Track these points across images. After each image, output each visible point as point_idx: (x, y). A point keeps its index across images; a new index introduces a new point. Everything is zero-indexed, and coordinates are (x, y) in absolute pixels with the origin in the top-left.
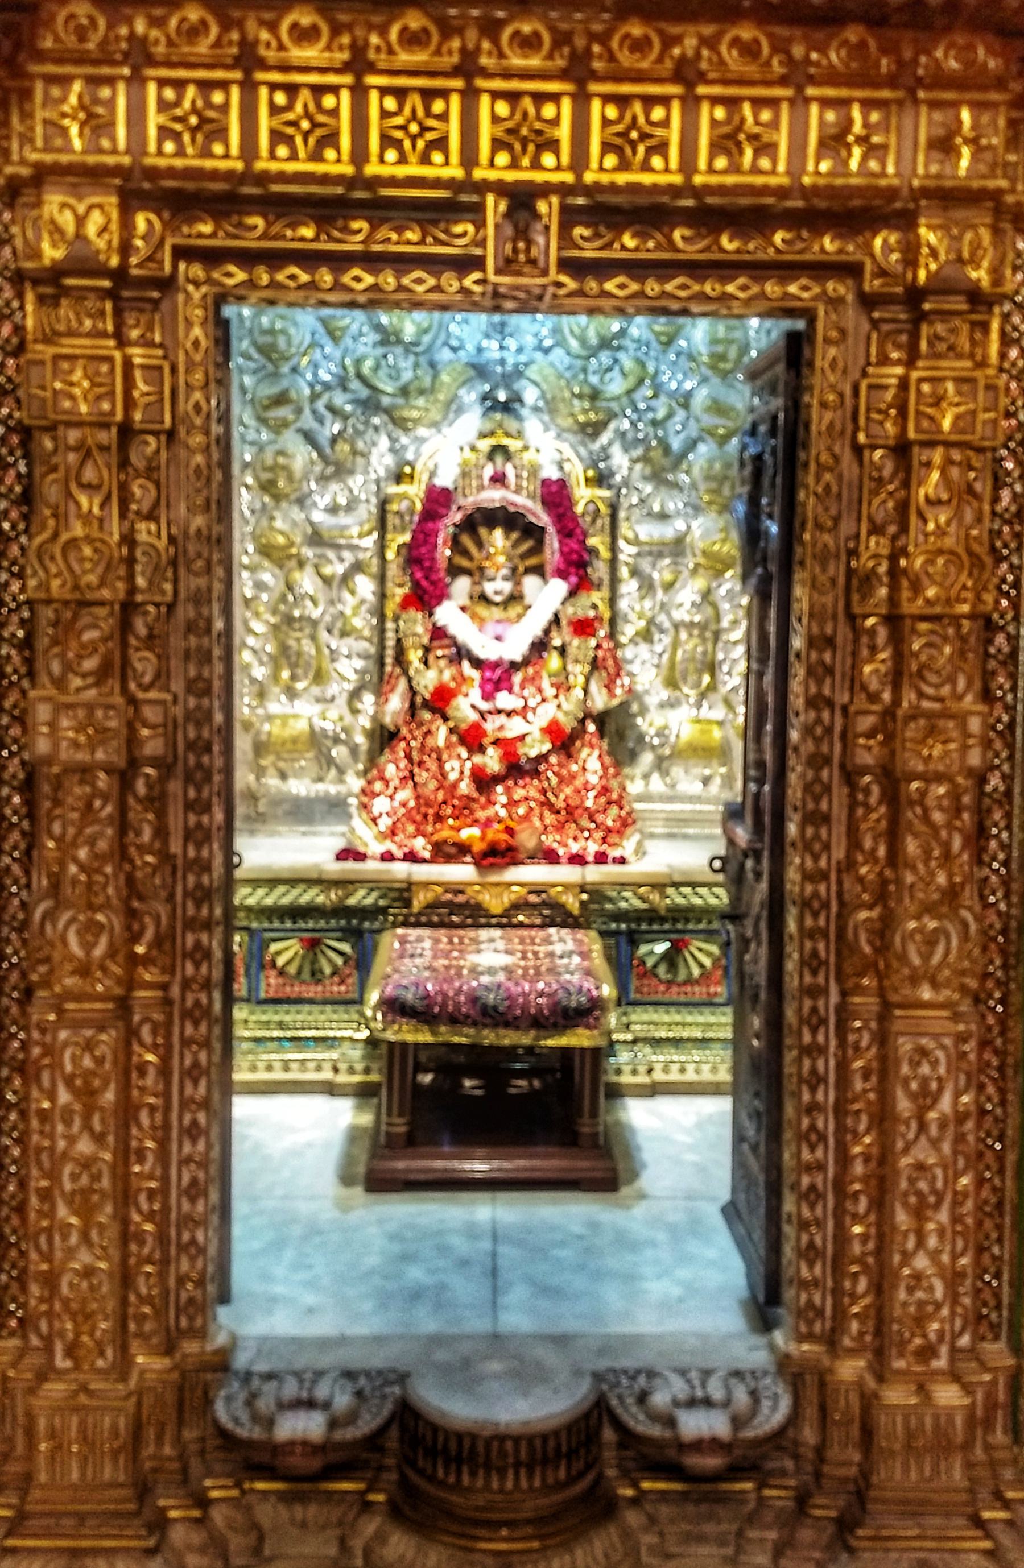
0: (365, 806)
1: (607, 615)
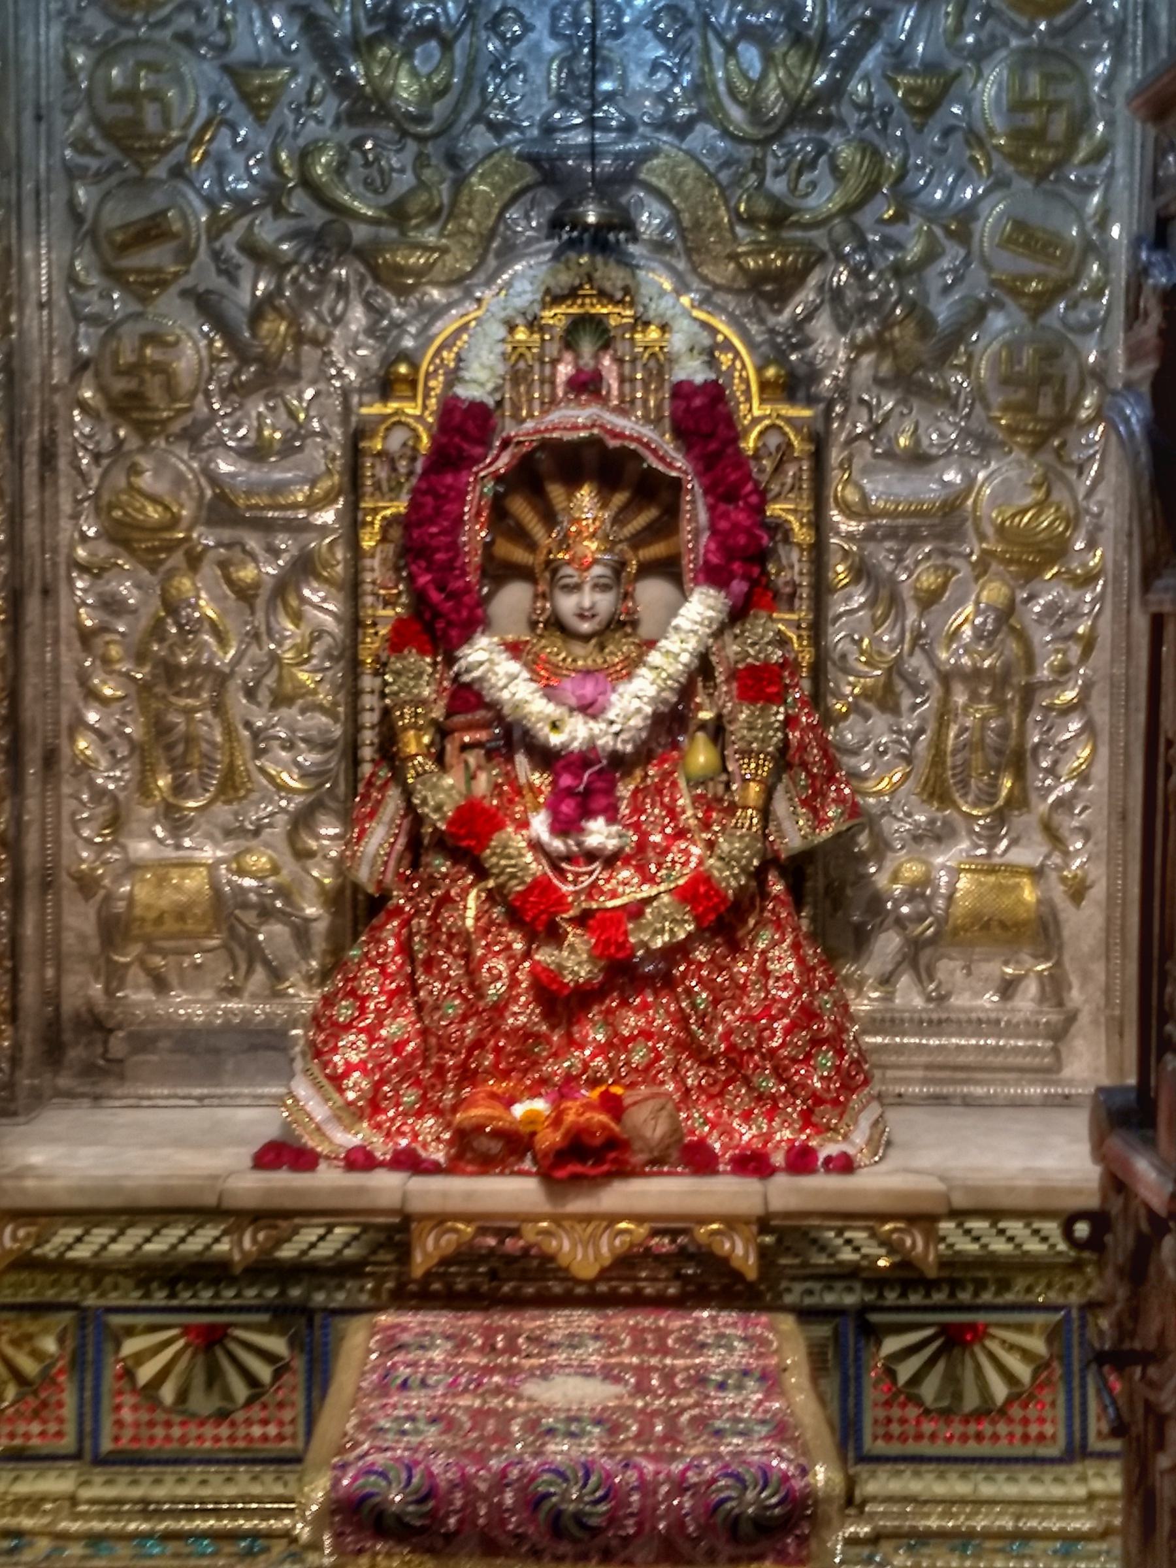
0: (317, 1052)
1: (806, 658)
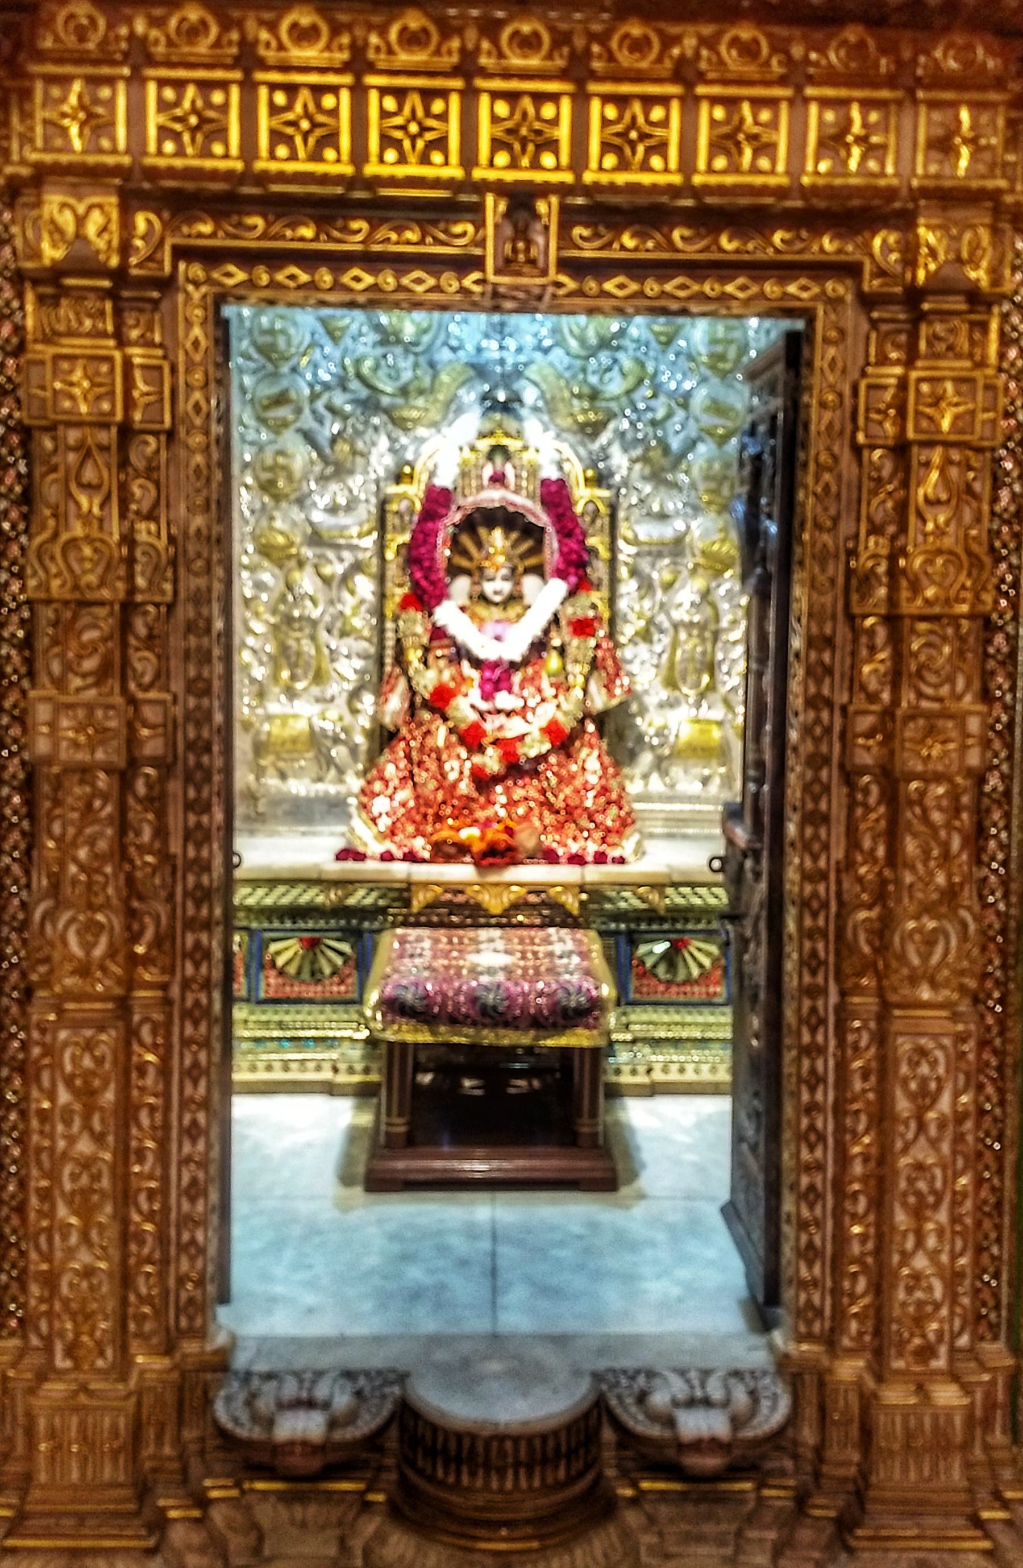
0: (364, 806)
1: (606, 615)
